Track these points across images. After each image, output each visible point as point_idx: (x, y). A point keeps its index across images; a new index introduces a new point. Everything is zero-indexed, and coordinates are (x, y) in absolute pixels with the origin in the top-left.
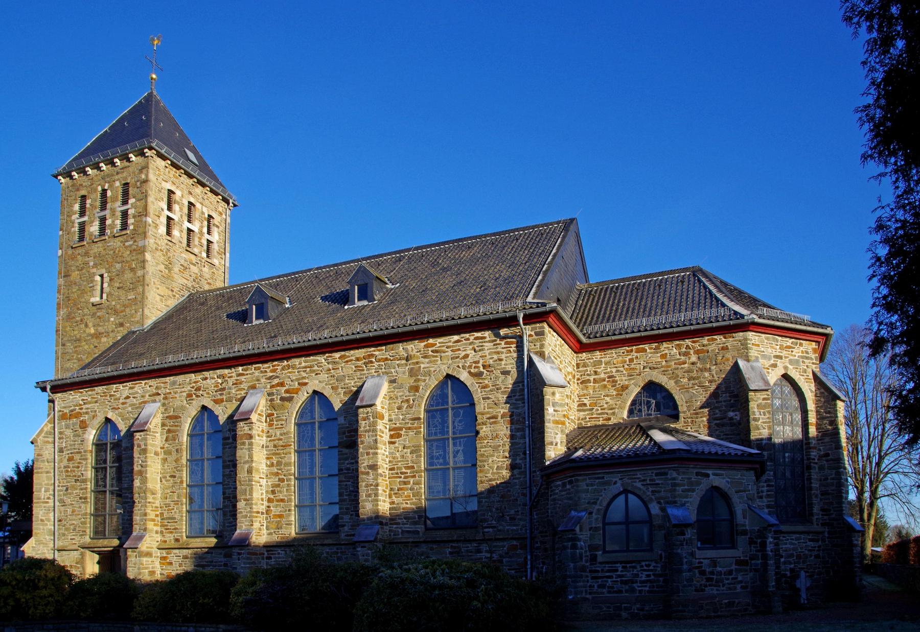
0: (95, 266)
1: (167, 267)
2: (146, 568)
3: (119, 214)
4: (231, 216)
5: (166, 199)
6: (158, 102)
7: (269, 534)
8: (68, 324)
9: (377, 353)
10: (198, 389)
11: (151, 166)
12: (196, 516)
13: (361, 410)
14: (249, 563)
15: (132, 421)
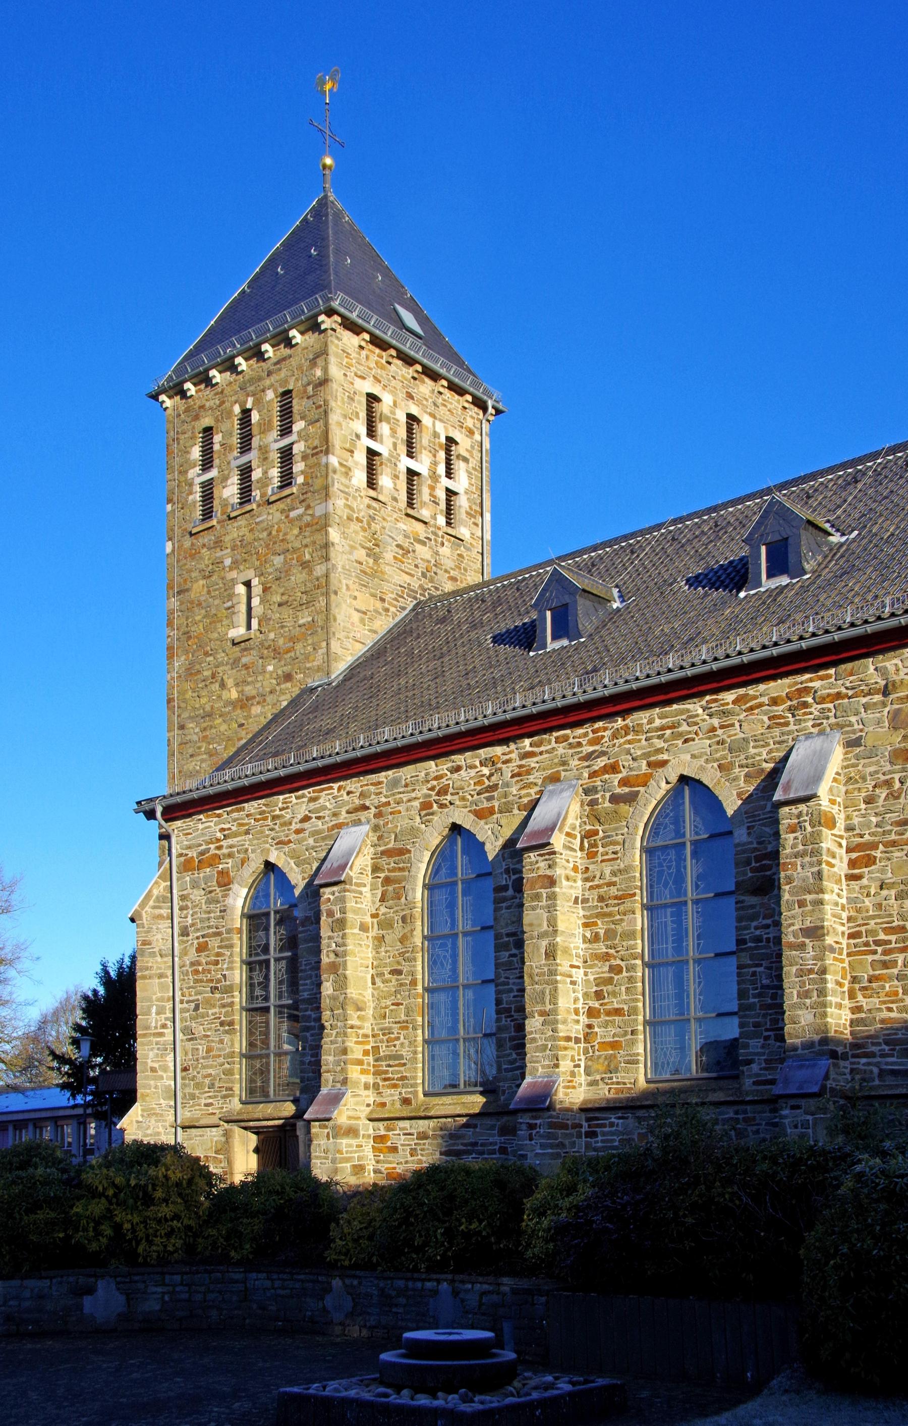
0: (235, 565)
1: (370, 553)
2: (347, 1160)
3: (275, 456)
4: (491, 435)
5: (363, 414)
6: (338, 215)
7: (591, 1084)
8: (188, 686)
9: (816, 684)
10: (443, 791)
11: (332, 349)
12: (442, 1050)
13: (785, 810)
14: (551, 1146)
15: (315, 865)
